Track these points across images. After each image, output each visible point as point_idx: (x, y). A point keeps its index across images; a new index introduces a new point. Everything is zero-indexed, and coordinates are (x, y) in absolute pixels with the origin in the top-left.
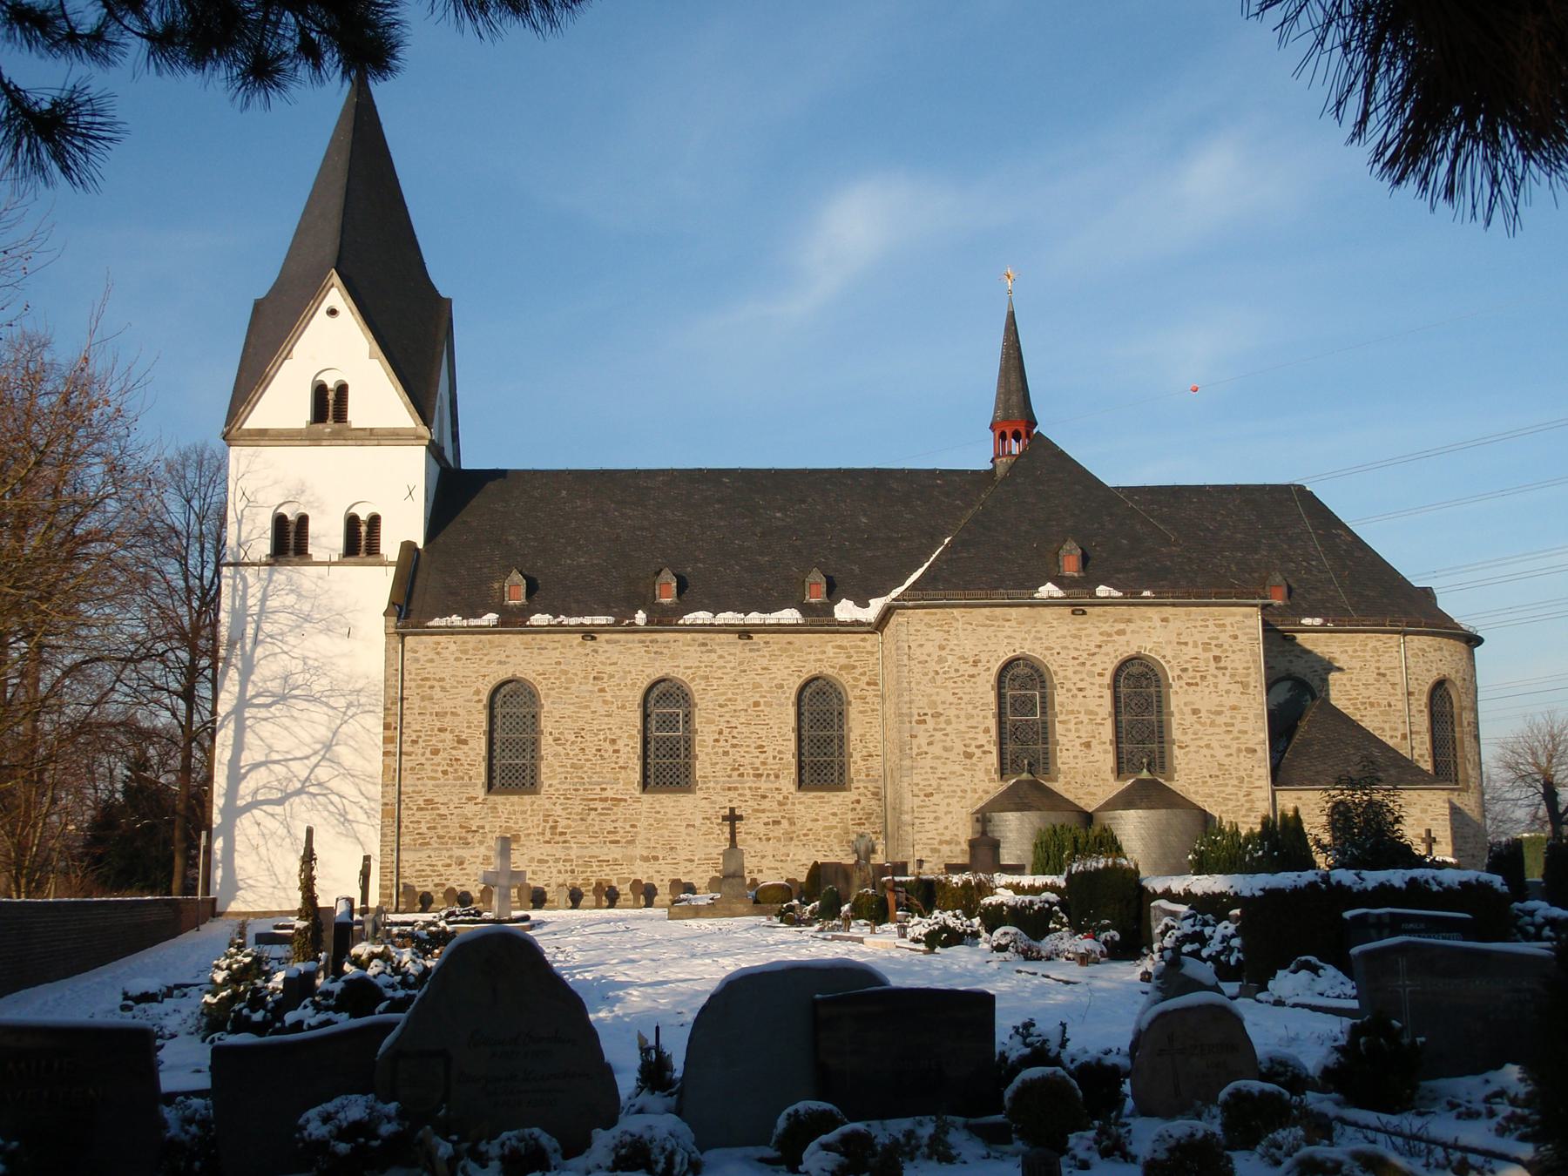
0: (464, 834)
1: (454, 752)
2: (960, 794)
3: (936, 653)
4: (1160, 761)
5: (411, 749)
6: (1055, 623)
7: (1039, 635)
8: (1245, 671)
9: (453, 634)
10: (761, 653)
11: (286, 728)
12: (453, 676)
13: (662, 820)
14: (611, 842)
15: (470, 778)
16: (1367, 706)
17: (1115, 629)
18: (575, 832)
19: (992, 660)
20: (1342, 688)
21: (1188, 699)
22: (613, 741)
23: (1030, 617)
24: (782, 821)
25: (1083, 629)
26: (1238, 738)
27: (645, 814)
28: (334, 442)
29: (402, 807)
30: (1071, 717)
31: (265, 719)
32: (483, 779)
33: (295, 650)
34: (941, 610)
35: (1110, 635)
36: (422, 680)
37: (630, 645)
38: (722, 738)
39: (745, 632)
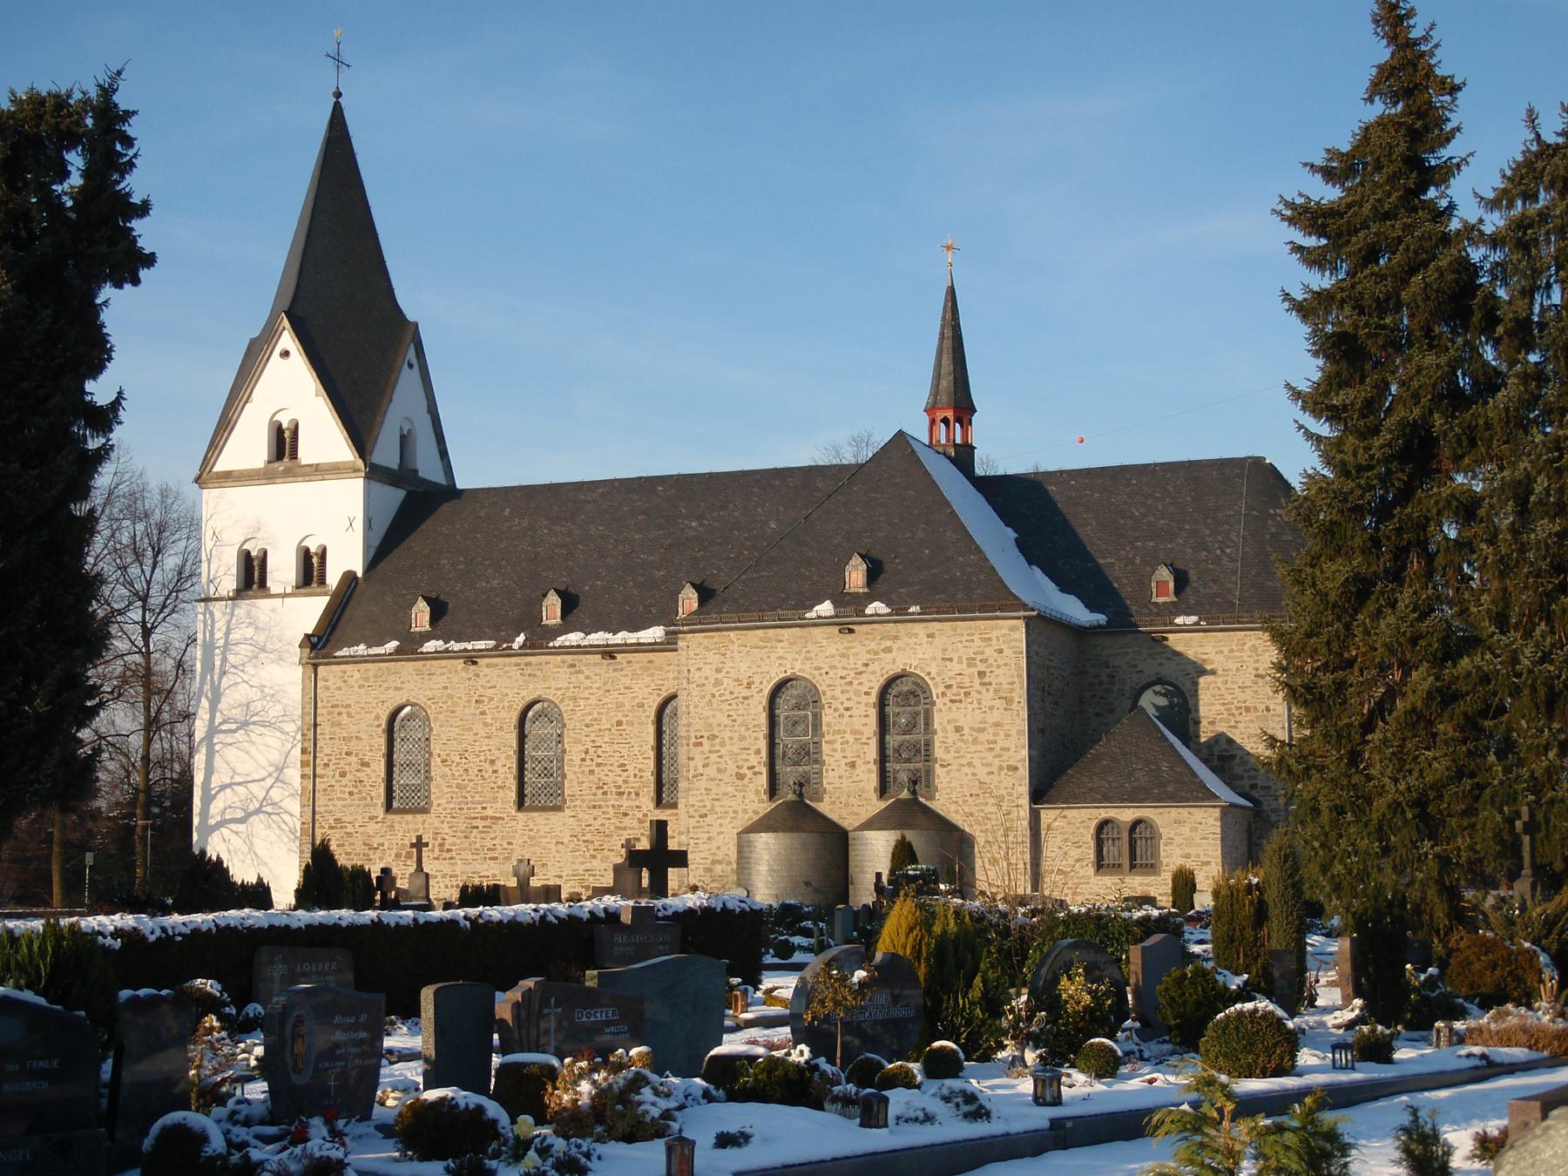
0: (367, 851)
1: (358, 774)
2: (732, 815)
3: (713, 676)
4: (921, 780)
5: (323, 772)
6: (824, 643)
7: (809, 655)
8: (1009, 686)
9: (356, 662)
10: (624, 672)
11: (247, 753)
12: (358, 702)
13: (534, 838)
14: (491, 859)
15: (372, 798)
16: (1243, 710)
17: (882, 647)
18: (459, 849)
19: (765, 682)
20: (1218, 692)
21: (952, 716)
22: (492, 762)
23: (802, 637)
24: (642, 838)
25: (850, 648)
26: (1000, 756)
27: (520, 832)
28: (286, 480)
29: (317, 825)
30: (838, 736)
31: (231, 744)
32: (382, 799)
33: (254, 679)
34: (719, 633)
35: (876, 653)
36: (332, 707)
37: (507, 669)
38: (588, 757)
39: (609, 653)
